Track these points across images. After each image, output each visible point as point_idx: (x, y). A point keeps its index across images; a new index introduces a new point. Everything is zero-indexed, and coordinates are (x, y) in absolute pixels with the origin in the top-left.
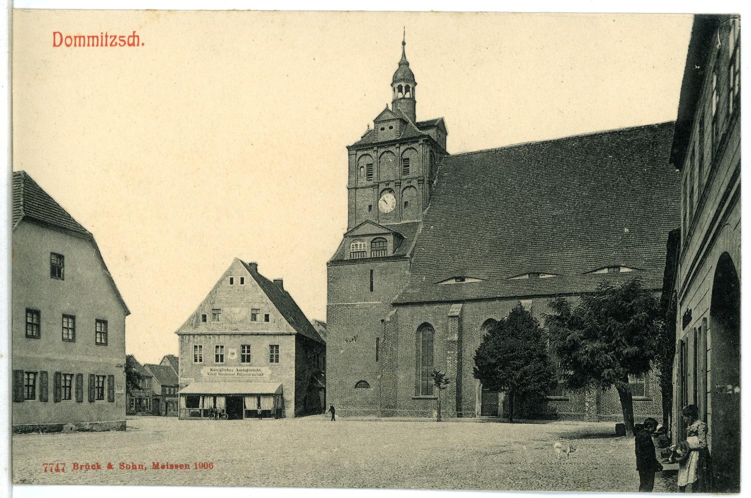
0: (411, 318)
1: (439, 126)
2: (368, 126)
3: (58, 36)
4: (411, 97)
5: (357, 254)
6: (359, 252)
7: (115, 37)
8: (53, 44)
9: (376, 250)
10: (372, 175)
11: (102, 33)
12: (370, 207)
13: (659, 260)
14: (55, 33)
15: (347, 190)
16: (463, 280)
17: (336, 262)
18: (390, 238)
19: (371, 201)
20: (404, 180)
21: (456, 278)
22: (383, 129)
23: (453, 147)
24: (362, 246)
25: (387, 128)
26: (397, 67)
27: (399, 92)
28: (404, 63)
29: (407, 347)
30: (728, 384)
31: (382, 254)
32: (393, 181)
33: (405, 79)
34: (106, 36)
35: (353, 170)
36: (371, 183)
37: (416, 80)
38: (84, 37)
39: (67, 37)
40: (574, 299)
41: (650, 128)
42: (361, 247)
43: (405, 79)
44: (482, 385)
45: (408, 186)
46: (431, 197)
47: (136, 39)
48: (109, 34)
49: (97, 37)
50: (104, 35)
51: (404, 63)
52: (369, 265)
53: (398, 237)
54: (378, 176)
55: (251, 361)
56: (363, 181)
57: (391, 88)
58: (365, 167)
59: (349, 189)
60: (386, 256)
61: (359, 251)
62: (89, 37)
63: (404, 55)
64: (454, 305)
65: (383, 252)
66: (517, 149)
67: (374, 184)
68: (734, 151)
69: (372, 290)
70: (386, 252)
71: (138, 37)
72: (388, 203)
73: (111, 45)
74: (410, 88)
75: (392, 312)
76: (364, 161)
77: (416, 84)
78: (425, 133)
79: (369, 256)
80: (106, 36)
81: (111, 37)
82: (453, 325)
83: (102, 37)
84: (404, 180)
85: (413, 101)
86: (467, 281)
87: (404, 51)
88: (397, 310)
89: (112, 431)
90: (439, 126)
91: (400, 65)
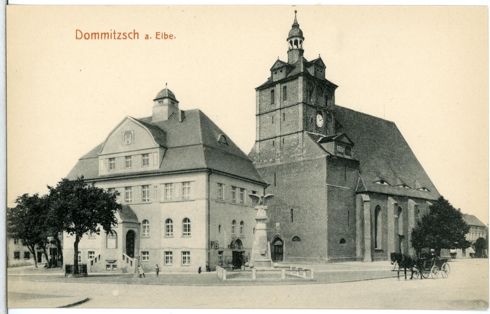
1: (319, 64)
7: (120, 34)
8: (75, 37)
13: (222, 270)
28: (296, 26)
30: (178, 109)
33: (296, 36)
34: (115, 33)
37: (304, 36)
38: (98, 33)
39: (85, 34)
40: (8, 214)
43: (296, 36)
47: (136, 35)
48: (116, 32)
49: (108, 33)
50: (113, 32)
51: (296, 26)
55: (232, 252)
68: (409, 188)
71: (138, 33)
77: (303, 39)
80: (115, 33)
85: (301, 51)
89: (408, 196)
90: (319, 64)
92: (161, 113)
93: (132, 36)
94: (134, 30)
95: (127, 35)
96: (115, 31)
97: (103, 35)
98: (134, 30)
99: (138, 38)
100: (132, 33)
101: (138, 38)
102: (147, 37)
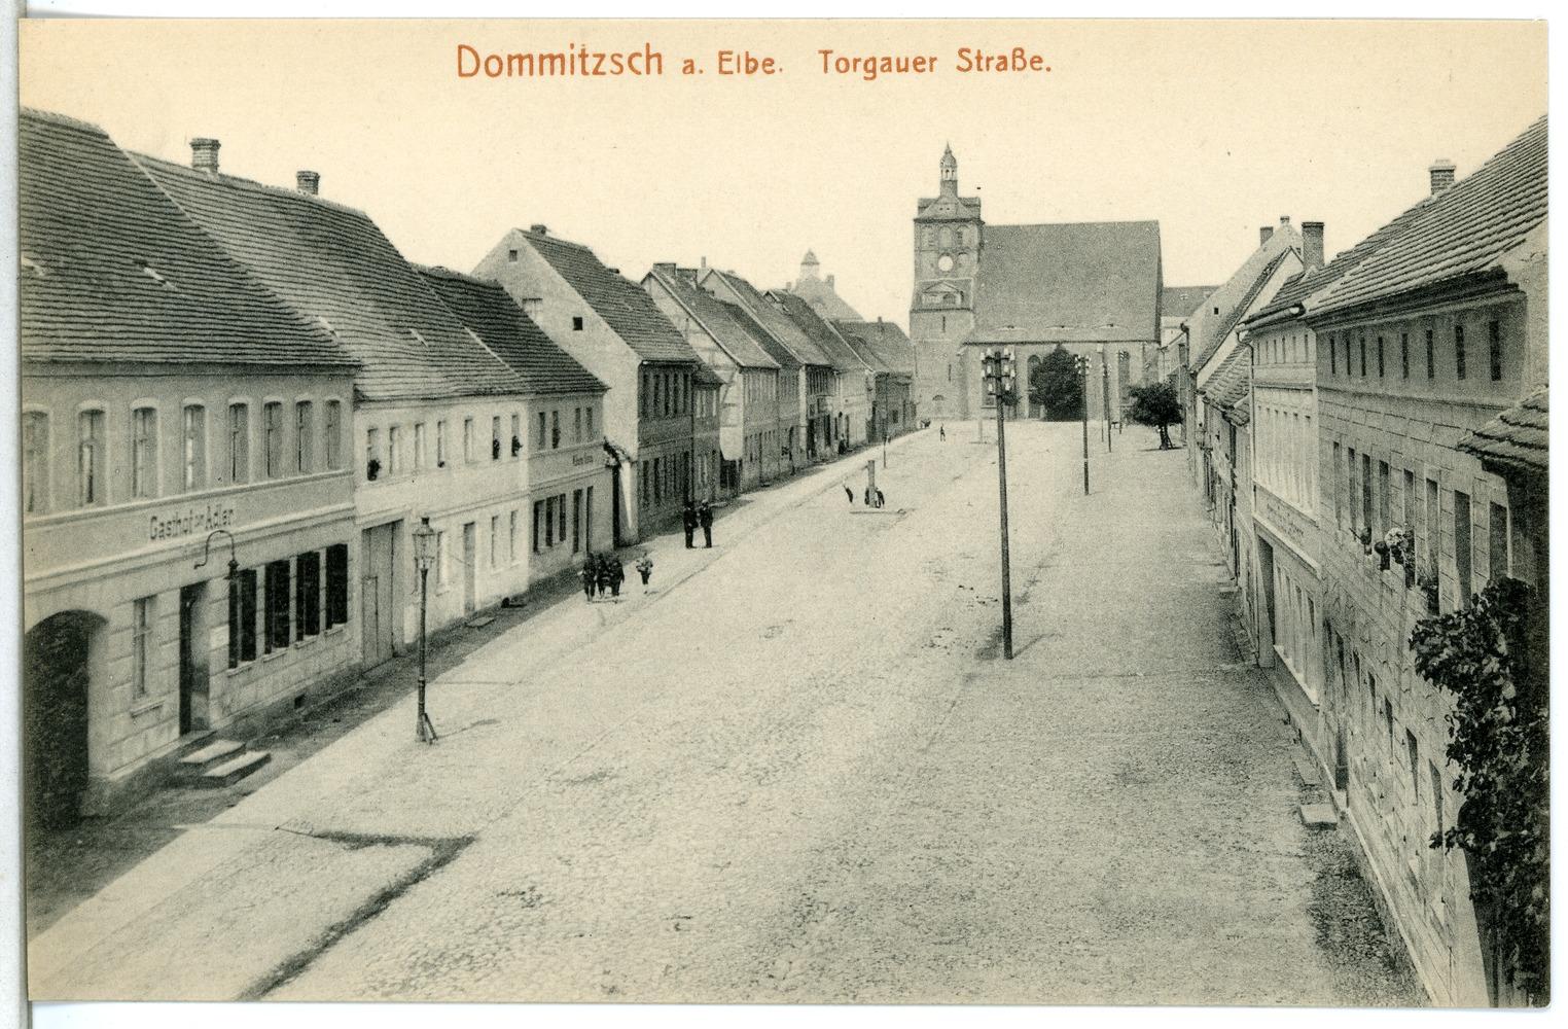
1: (973, 204)
3: (467, 55)
11: (572, 46)
28: (948, 152)
31: (952, 305)
33: (949, 161)
43: (949, 161)
47: (654, 62)
49: (561, 57)
51: (948, 152)
62: (542, 58)
71: (659, 56)
73: (596, 72)
90: (973, 204)
92: (1277, 225)
93: (639, 63)
95: (624, 61)
96: (979, 52)
97: (515, 63)
99: (660, 71)
101: (660, 71)
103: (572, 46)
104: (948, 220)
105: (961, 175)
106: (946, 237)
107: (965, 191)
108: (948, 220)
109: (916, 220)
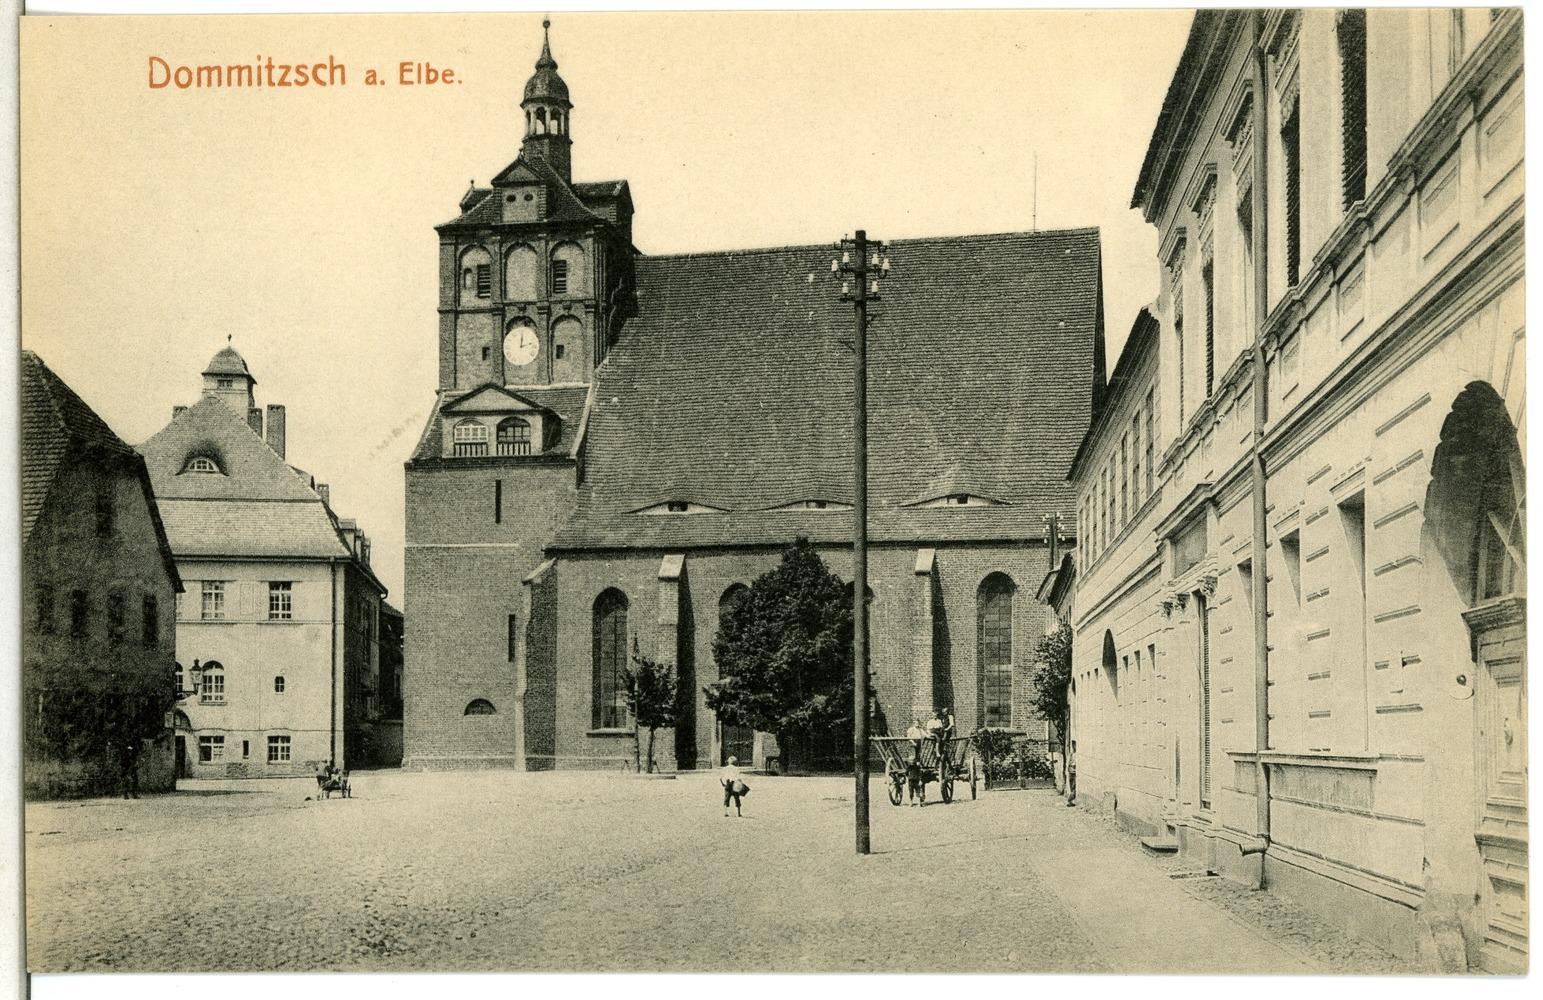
0: (579, 584)
1: (619, 198)
2: (472, 182)
4: (563, 133)
5: (468, 447)
6: (474, 444)
9: (509, 443)
10: (488, 287)
11: (259, 58)
12: (485, 350)
14: (152, 59)
15: (438, 316)
16: (684, 508)
17: (425, 464)
18: (537, 422)
19: (486, 338)
20: (555, 302)
21: (671, 505)
22: (512, 199)
23: (651, 236)
24: (479, 431)
25: (520, 198)
26: (533, 71)
27: (552, 119)
28: (547, 65)
29: (574, 638)
31: (518, 451)
32: (581, 301)
33: (549, 95)
35: (453, 276)
36: (486, 303)
41: (758, 253)
42: (483, 434)
43: (549, 95)
44: (720, 722)
45: (563, 316)
46: (610, 338)
47: (338, 73)
49: (249, 68)
50: (264, 63)
51: (547, 65)
52: (490, 474)
53: (551, 419)
54: (504, 292)
56: (469, 299)
57: (522, 113)
58: (475, 271)
59: (440, 312)
60: (527, 454)
61: (471, 441)
62: (230, 69)
63: (547, 50)
64: (922, 551)
65: (506, 446)
66: (773, 256)
67: (493, 306)
69: (498, 521)
70: (527, 446)
72: (523, 346)
74: (545, 112)
75: (546, 565)
76: (473, 259)
78: (597, 212)
79: (493, 453)
81: (281, 67)
82: (669, 595)
83: (259, 68)
84: (555, 302)
86: (692, 510)
87: (547, 39)
88: (555, 564)
90: (619, 198)
91: (539, 66)
93: (324, 75)
94: (332, 58)
98: (332, 58)
99: (343, 81)
100: (324, 66)
101: (343, 81)
102: (371, 78)
103: (259, 58)
104: (544, 224)
105: (580, 127)
106: (523, 275)
107: (587, 167)
108: (544, 224)
109: (443, 231)
